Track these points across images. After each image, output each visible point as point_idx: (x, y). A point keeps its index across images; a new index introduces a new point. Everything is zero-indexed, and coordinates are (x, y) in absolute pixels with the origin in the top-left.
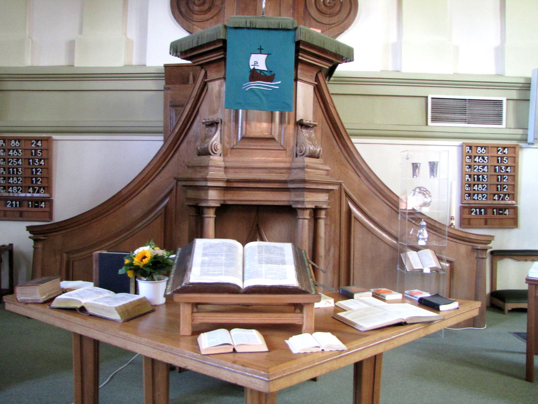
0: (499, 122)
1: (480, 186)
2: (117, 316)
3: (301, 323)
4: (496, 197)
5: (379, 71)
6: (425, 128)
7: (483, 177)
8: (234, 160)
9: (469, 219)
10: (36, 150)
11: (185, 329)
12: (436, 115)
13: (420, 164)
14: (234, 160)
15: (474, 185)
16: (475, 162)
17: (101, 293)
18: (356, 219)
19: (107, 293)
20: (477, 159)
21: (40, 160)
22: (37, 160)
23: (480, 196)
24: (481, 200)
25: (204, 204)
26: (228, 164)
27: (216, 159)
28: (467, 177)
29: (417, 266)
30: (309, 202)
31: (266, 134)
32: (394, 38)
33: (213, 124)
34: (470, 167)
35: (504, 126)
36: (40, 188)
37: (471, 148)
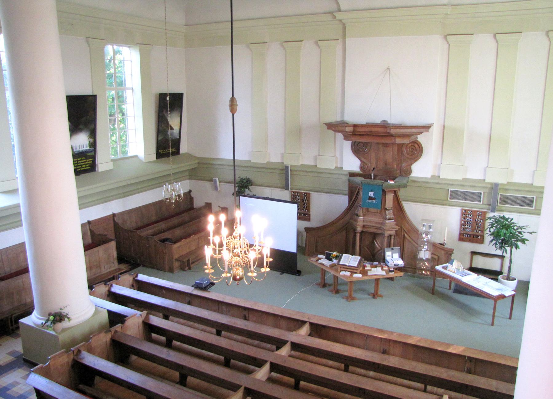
0: (480, 201)
1: (468, 226)
2: (329, 266)
4: (475, 231)
5: (429, 176)
7: (470, 223)
9: (463, 238)
11: (339, 270)
15: (466, 225)
16: (467, 216)
17: (326, 261)
18: (406, 238)
19: (327, 261)
20: (467, 215)
21: (306, 200)
23: (468, 230)
24: (469, 232)
27: (361, 218)
28: (463, 222)
29: (421, 257)
32: (439, 162)
34: (464, 218)
35: (481, 203)
37: (465, 211)
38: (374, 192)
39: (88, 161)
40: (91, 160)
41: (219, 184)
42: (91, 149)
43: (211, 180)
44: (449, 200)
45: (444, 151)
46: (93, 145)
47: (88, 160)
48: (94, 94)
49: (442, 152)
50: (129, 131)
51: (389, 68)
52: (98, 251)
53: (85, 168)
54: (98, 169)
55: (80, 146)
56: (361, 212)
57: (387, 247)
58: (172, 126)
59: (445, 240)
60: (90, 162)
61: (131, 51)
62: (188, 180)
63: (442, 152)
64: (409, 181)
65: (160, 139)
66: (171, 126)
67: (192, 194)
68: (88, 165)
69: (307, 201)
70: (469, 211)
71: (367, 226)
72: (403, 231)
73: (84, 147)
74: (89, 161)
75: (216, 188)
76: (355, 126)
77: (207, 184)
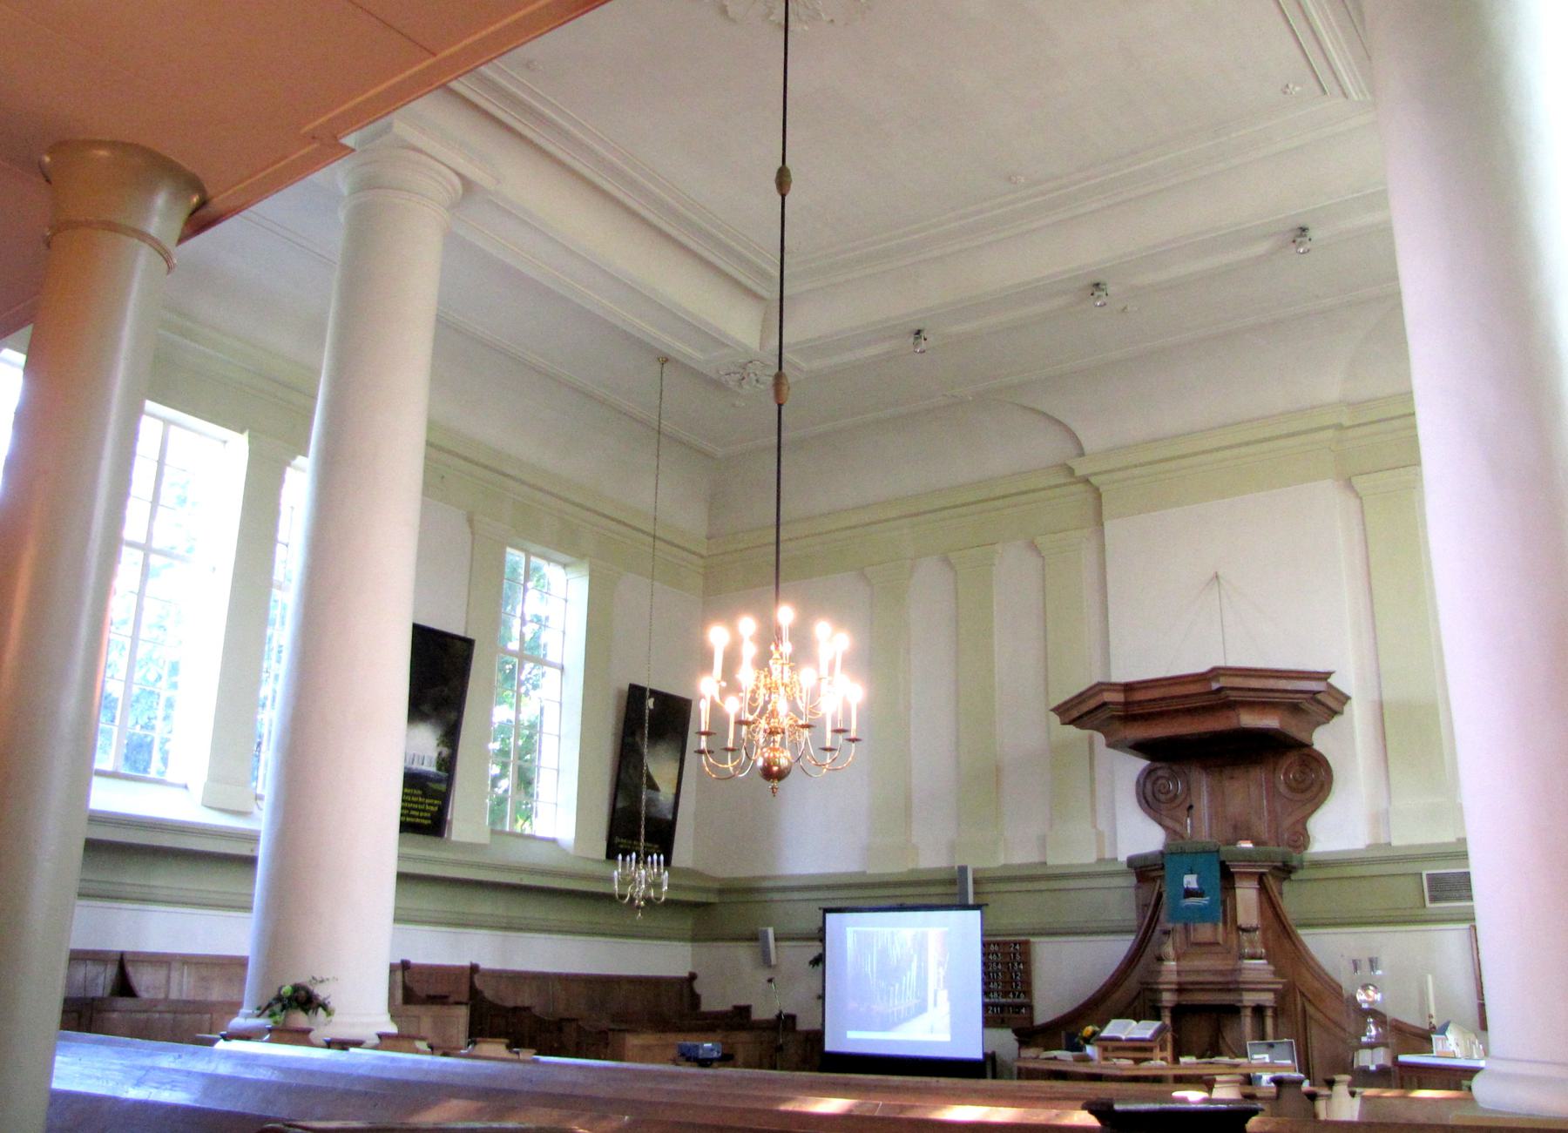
3: (818, 1027)
6: (1421, 912)
8: (1187, 964)
10: (1014, 955)
12: (1435, 894)
13: (1360, 961)
14: (1187, 964)
18: (1311, 1018)
21: (1019, 964)
22: (1016, 965)
25: (1159, 1005)
26: (1181, 969)
27: (1171, 964)
30: (1249, 1000)
31: (1212, 940)
33: (1167, 933)
36: (1020, 993)
38: (1198, 874)
39: (430, 804)
40: (436, 802)
41: (776, 947)
42: (440, 773)
43: (755, 938)
44: (1428, 904)
45: (1391, 768)
46: (448, 764)
47: (428, 801)
48: (469, 637)
49: (1387, 771)
50: (542, 770)
51: (1217, 577)
52: (418, 1017)
53: (418, 820)
54: (450, 834)
55: (414, 755)
56: (1169, 949)
57: (1253, 1039)
58: (657, 781)
59: (1431, 1017)
60: (432, 808)
61: (570, 576)
62: (689, 944)
63: (1387, 771)
64: (1305, 864)
65: (620, 805)
66: (650, 778)
67: (699, 987)
68: (426, 814)
69: (1021, 967)
70: (992, 946)
71: (1190, 987)
72: (1299, 998)
73: (425, 762)
74: (432, 806)
75: (765, 960)
76: (1128, 687)
77: (743, 953)
